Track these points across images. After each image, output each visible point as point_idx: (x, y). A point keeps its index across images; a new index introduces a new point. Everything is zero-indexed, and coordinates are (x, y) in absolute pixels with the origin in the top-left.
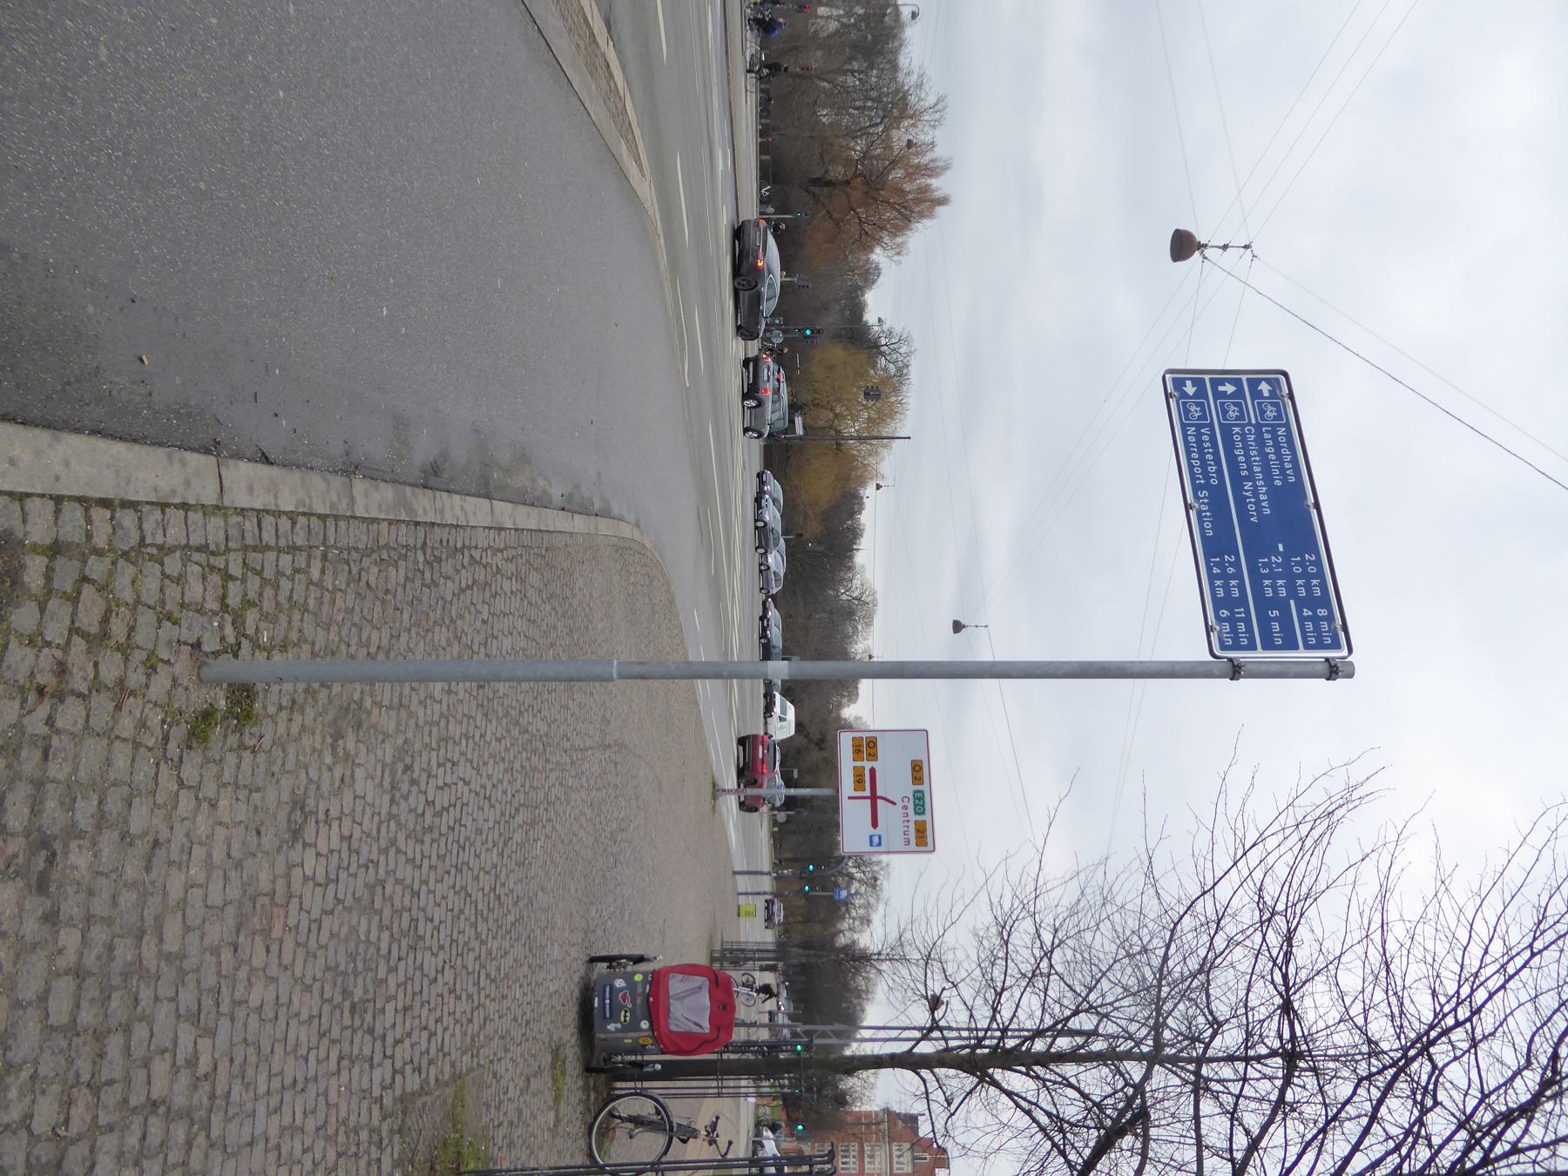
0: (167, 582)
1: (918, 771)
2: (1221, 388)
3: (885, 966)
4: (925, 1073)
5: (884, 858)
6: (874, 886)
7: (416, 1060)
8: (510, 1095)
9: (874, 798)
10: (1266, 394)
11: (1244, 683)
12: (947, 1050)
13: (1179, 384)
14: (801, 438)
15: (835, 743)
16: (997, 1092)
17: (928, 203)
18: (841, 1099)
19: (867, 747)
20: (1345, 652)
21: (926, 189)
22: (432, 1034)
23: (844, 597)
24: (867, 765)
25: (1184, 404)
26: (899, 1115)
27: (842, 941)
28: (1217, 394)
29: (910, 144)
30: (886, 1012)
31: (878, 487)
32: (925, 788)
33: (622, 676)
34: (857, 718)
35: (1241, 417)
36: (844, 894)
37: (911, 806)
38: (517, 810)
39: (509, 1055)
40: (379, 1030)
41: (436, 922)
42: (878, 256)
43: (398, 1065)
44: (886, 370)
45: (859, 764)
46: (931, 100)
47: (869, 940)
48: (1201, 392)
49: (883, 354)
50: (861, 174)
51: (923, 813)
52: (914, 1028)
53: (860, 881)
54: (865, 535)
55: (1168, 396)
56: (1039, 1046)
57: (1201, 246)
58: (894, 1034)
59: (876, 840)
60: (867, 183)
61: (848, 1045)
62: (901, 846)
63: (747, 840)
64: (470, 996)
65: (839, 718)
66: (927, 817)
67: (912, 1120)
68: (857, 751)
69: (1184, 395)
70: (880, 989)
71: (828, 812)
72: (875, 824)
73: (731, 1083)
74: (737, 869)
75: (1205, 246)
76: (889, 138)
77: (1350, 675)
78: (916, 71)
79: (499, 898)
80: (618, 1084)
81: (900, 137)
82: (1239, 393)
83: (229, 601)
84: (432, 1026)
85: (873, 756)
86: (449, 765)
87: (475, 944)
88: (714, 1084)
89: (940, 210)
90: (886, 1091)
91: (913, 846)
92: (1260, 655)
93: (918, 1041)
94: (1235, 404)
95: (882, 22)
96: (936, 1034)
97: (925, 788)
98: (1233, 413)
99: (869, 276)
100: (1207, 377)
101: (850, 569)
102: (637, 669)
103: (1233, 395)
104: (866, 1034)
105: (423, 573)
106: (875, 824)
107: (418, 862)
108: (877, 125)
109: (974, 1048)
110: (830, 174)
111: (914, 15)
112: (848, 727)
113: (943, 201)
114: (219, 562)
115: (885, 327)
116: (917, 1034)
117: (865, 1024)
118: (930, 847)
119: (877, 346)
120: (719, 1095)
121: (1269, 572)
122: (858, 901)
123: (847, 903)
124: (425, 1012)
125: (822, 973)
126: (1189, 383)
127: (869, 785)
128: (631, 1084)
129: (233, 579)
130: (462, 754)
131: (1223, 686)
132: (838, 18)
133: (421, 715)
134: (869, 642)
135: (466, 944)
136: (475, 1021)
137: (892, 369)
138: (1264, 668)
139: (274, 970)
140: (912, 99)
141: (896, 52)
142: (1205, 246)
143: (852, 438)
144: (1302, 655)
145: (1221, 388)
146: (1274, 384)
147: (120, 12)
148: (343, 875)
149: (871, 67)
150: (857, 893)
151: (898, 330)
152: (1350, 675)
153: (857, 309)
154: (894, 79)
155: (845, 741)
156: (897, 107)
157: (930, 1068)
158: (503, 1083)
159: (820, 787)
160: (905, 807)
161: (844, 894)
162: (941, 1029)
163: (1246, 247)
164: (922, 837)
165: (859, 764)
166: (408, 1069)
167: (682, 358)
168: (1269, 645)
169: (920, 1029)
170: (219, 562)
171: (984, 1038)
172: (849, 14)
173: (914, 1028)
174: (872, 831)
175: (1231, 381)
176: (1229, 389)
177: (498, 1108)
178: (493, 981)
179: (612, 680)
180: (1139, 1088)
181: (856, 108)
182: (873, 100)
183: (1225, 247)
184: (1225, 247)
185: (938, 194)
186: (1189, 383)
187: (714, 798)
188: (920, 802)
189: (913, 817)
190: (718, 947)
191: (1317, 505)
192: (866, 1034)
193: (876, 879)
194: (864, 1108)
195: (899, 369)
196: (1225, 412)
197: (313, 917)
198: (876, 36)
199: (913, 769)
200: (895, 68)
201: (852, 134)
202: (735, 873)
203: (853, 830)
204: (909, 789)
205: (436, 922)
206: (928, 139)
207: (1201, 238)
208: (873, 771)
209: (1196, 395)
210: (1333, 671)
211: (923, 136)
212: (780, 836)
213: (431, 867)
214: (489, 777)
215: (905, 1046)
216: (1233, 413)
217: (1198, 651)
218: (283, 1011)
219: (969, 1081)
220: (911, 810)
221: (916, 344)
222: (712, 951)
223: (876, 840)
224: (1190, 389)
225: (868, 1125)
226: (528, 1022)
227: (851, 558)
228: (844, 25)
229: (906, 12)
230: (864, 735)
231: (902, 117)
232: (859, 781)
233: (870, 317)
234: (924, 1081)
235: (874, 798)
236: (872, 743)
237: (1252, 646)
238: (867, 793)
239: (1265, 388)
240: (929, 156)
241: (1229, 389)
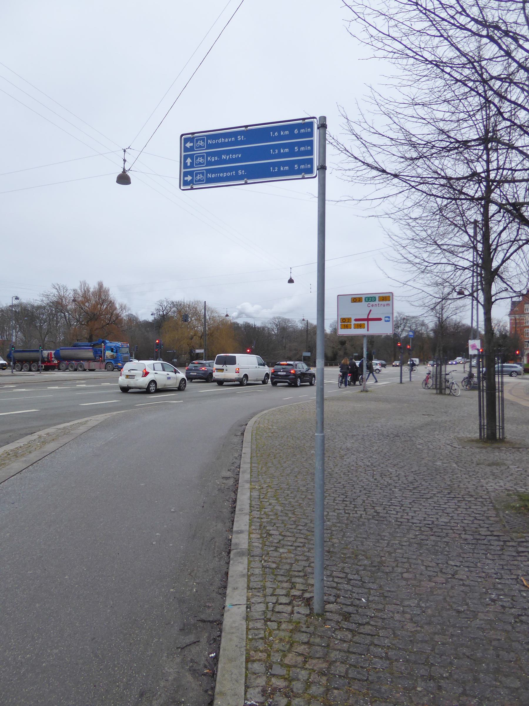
0: (280, 628)
1: (356, 299)
2: (189, 164)
3: (445, 316)
4: (493, 299)
5: (395, 314)
6: (407, 320)
7: (487, 526)
8: (502, 484)
9: (368, 320)
10: (192, 144)
11: (328, 164)
12: (483, 290)
13: (186, 183)
14: (205, 351)
15: (342, 336)
16: (502, 267)
17: (101, 293)
18: (504, 336)
19: (345, 322)
20: (315, 120)
21: (94, 294)
22: (476, 518)
23: (276, 332)
24: (353, 322)
25: (196, 181)
26: (512, 310)
27: (432, 334)
28: (192, 166)
29: (74, 301)
30: (466, 314)
31: (227, 316)
32: (364, 297)
33: (322, 431)
34: (331, 326)
35: (203, 157)
36: (411, 333)
37: (372, 303)
38: (376, 479)
39: (485, 485)
40: (474, 542)
41: (426, 516)
42: (124, 315)
43: (489, 533)
44: (174, 312)
45: (353, 326)
46: (55, 291)
47: (431, 322)
48: (191, 173)
49: (167, 314)
50: (87, 322)
51: (375, 298)
52: (472, 303)
53: (405, 326)
54: (249, 322)
55: (192, 189)
56: (480, 247)
57: (124, 171)
58: (475, 312)
59: (387, 319)
60: (91, 319)
61: (480, 332)
62: (389, 309)
63: (387, 376)
64: (459, 501)
65: (331, 335)
66: (377, 296)
67: (514, 304)
68: (347, 327)
69: (191, 182)
70: (455, 318)
71: (372, 340)
72: (380, 319)
73: (497, 386)
74: (399, 381)
75: (124, 169)
76: (70, 310)
77: (325, 118)
78: (41, 298)
79: (414, 488)
80: (498, 436)
81: (71, 306)
82: (191, 156)
83: (287, 602)
84: (472, 519)
85: (349, 320)
86: (356, 509)
87: (436, 499)
88: (497, 394)
89: (105, 285)
90: (501, 313)
91: (390, 302)
92: (316, 157)
93: (478, 302)
94: (197, 159)
95: (19, 313)
96: (475, 294)
97: (364, 297)
98: (201, 160)
99: (132, 319)
100: (183, 170)
101: (263, 328)
102: (319, 425)
103: (192, 159)
104: (475, 324)
105: (272, 519)
106: (380, 319)
107: (399, 523)
108: (65, 315)
109: (481, 277)
110: (82, 334)
111: (17, 298)
112: (335, 330)
113: (101, 285)
114: (270, 605)
115: (155, 312)
116: (475, 302)
117: (470, 325)
118: (390, 295)
119: (163, 316)
120: (502, 391)
121: (277, 151)
122: (414, 327)
123: (414, 332)
124: (465, 521)
125: (446, 342)
126: (186, 179)
127: (362, 322)
128: (498, 431)
129: (277, 600)
130: (351, 503)
131: (328, 172)
132: (17, 332)
133: (335, 521)
134: (297, 320)
135: (435, 502)
136: (469, 499)
137: (174, 309)
138: (321, 155)
139: (449, 586)
140: (55, 299)
141: (33, 307)
142: (124, 169)
143: (205, 328)
144: (316, 138)
145: (189, 164)
146: (186, 140)
147: (37, 644)
148: (406, 555)
149: (38, 318)
150: (410, 327)
151: (157, 307)
152: (325, 118)
153: (147, 324)
154: (44, 308)
155: (342, 332)
156: (58, 305)
157: (491, 297)
158: (497, 488)
159: (363, 345)
160: (372, 305)
161: (411, 333)
162: (473, 292)
163: (125, 151)
164: (386, 298)
165: (353, 326)
166: (491, 529)
167: (170, 404)
168: (311, 153)
169: (473, 300)
170: (270, 605)
171: (477, 272)
172: (15, 328)
173: (472, 303)
174: (383, 320)
175: (185, 159)
176: (189, 161)
177: (509, 490)
178: (451, 492)
179: (323, 437)
180: (501, 206)
181: (57, 324)
182: (53, 318)
183: (125, 161)
184: (125, 161)
185: (97, 286)
186: (186, 179)
187: (367, 391)
188: (370, 299)
189: (377, 302)
190: (434, 391)
191: (246, 126)
192: (475, 324)
193: (404, 319)
194: (509, 325)
195: (174, 306)
196: (200, 163)
197: (424, 569)
198: (24, 316)
199: (355, 302)
200: (39, 307)
201: (69, 325)
202: (401, 382)
203: (381, 329)
204: (364, 304)
205: (426, 516)
206: (72, 293)
207: (120, 171)
208: (356, 320)
209: (192, 176)
210: (323, 126)
211: (70, 295)
212: (388, 361)
213: (401, 518)
214: (360, 491)
215: (480, 307)
216: (201, 160)
217: (315, 182)
218: (466, 583)
219: (497, 279)
220: (374, 303)
221: (163, 298)
222: (437, 394)
223: (387, 319)
224: (189, 178)
225: (516, 324)
226: (470, 476)
227: (259, 328)
228: (20, 330)
229: (16, 302)
230: (340, 324)
231: (61, 304)
232: (360, 326)
233: (150, 319)
234: (496, 300)
235: (368, 320)
236: (343, 320)
237: (311, 161)
238: (366, 322)
239: (189, 145)
240: (79, 291)
241: (189, 161)
